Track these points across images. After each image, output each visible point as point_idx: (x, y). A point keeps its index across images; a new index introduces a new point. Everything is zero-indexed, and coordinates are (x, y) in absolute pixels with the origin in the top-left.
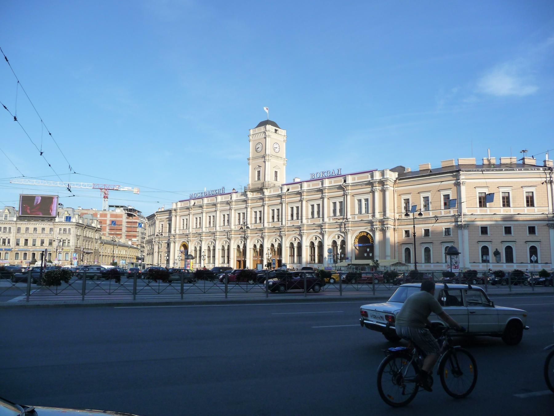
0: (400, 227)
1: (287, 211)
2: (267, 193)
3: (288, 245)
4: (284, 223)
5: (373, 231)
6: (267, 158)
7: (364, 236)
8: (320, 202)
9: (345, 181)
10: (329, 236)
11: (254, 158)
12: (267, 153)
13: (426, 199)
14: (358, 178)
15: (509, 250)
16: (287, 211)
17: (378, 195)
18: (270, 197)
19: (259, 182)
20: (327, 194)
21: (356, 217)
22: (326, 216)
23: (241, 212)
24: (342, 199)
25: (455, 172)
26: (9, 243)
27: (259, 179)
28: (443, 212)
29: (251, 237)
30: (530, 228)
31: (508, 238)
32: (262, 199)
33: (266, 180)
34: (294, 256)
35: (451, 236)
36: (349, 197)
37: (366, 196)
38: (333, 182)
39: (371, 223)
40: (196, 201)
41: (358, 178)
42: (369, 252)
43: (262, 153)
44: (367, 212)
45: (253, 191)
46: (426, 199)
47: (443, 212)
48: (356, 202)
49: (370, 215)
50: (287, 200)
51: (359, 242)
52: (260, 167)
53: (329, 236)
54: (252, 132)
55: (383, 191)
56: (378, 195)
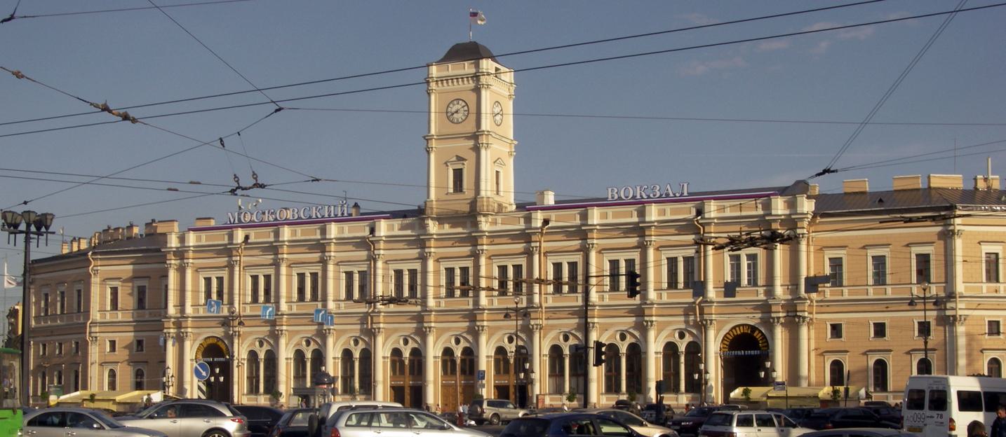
0: (819, 316)
1: (242, 284)
2: (485, 225)
3: (244, 355)
4: (536, 299)
5: (769, 323)
6: (483, 140)
7: (744, 335)
8: (271, 271)
9: (700, 212)
10: (337, 340)
11: (442, 137)
12: (483, 127)
13: (880, 262)
14: (673, 212)
15: (881, 367)
16: (242, 284)
17: (372, 263)
18: (495, 236)
19: (459, 196)
20: (654, 238)
21: (108, 314)
22: (331, 297)
23: (405, 267)
24: (691, 252)
25: (940, 209)
26: (614, 276)
27: (458, 186)
28: (871, 290)
29: (718, 322)
30: (990, 323)
31: (879, 343)
32: (473, 241)
33: (483, 193)
34: (305, 376)
35: (144, 352)
36: (380, 264)
37: (518, 261)
38: (668, 211)
39: (765, 308)
40: (253, 233)
41: (615, 215)
42: (220, 375)
43: (470, 127)
44: (753, 281)
45: (441, 219)
46: (880, 262)
47: (871, 290)
48: (202, 282)
49: (761, 290)
50: (544, 245)
51: (204, 356)
52: (460, 159)
53: (337, 340)
54: (434, 71)
55: (182, 270)
56: (372, 263)
